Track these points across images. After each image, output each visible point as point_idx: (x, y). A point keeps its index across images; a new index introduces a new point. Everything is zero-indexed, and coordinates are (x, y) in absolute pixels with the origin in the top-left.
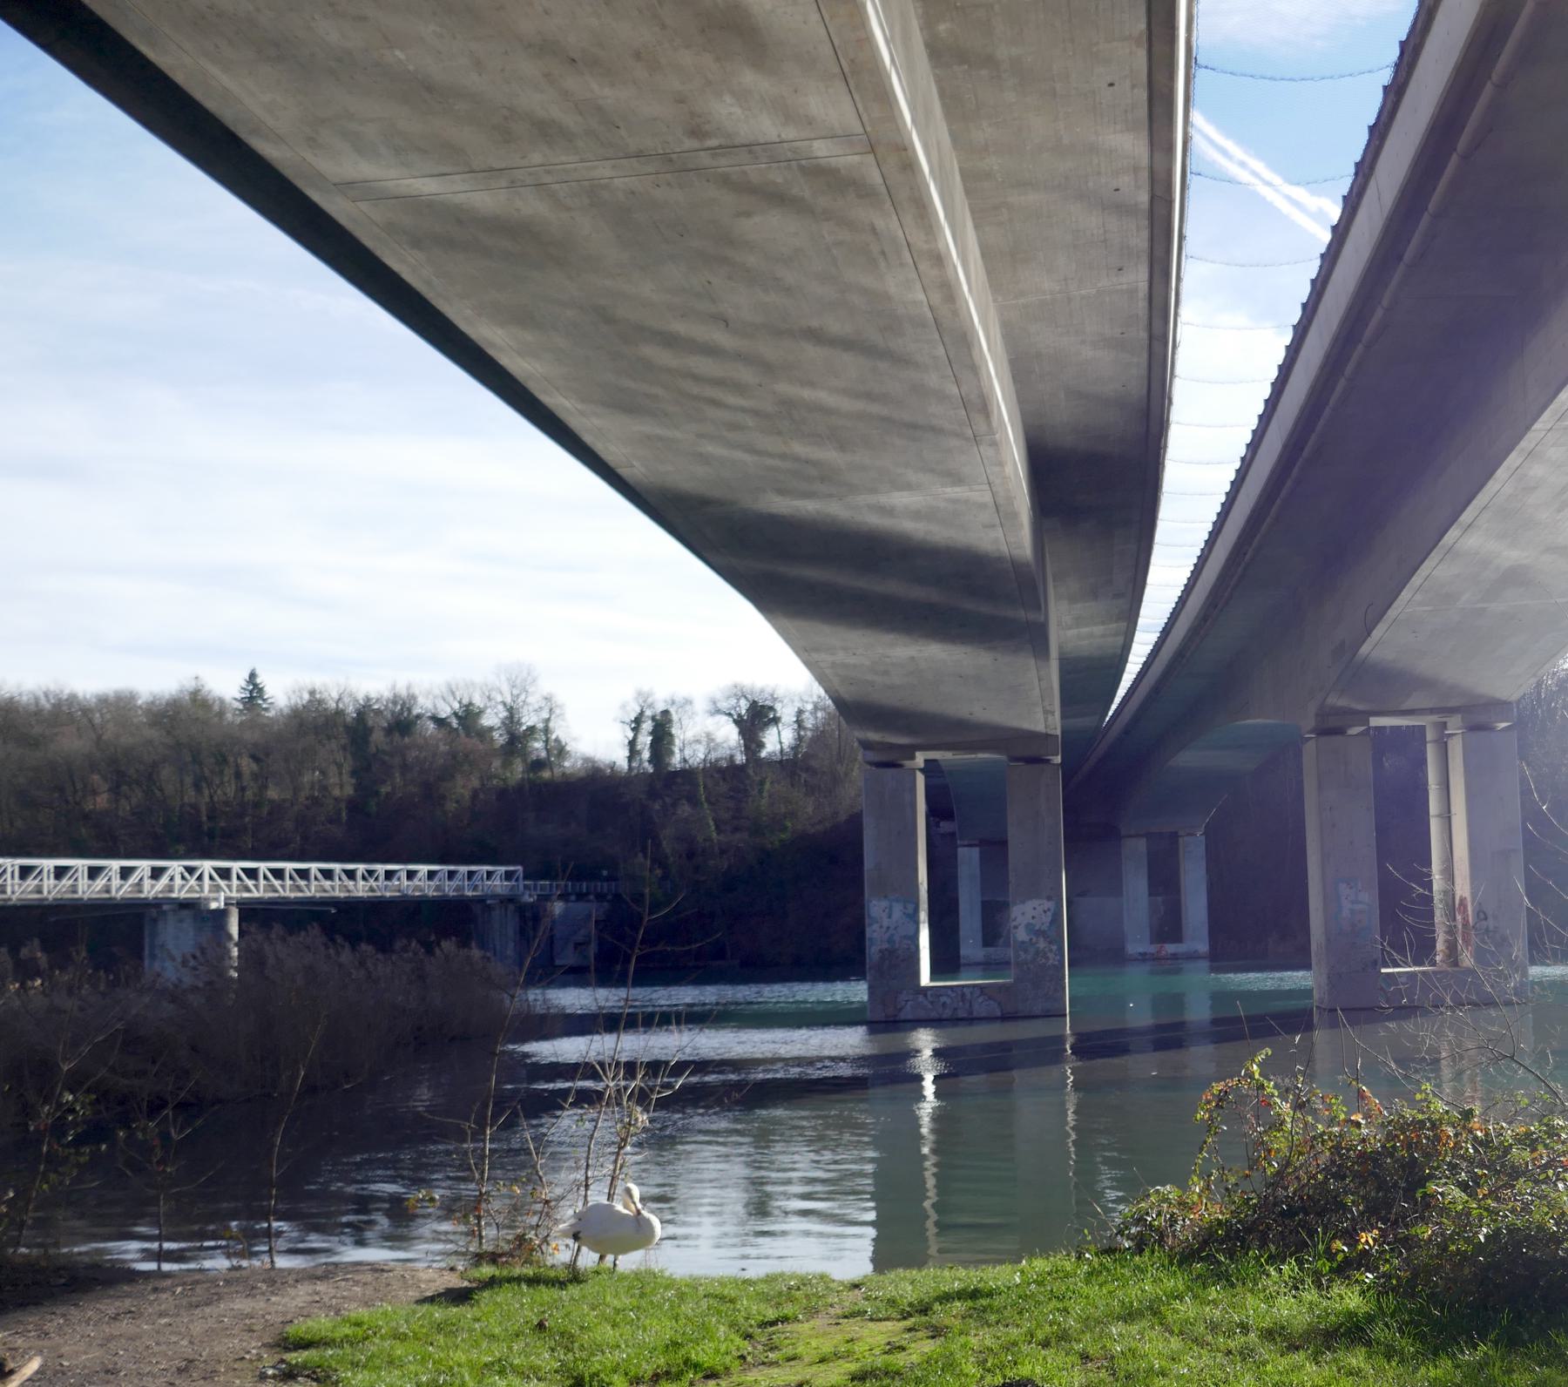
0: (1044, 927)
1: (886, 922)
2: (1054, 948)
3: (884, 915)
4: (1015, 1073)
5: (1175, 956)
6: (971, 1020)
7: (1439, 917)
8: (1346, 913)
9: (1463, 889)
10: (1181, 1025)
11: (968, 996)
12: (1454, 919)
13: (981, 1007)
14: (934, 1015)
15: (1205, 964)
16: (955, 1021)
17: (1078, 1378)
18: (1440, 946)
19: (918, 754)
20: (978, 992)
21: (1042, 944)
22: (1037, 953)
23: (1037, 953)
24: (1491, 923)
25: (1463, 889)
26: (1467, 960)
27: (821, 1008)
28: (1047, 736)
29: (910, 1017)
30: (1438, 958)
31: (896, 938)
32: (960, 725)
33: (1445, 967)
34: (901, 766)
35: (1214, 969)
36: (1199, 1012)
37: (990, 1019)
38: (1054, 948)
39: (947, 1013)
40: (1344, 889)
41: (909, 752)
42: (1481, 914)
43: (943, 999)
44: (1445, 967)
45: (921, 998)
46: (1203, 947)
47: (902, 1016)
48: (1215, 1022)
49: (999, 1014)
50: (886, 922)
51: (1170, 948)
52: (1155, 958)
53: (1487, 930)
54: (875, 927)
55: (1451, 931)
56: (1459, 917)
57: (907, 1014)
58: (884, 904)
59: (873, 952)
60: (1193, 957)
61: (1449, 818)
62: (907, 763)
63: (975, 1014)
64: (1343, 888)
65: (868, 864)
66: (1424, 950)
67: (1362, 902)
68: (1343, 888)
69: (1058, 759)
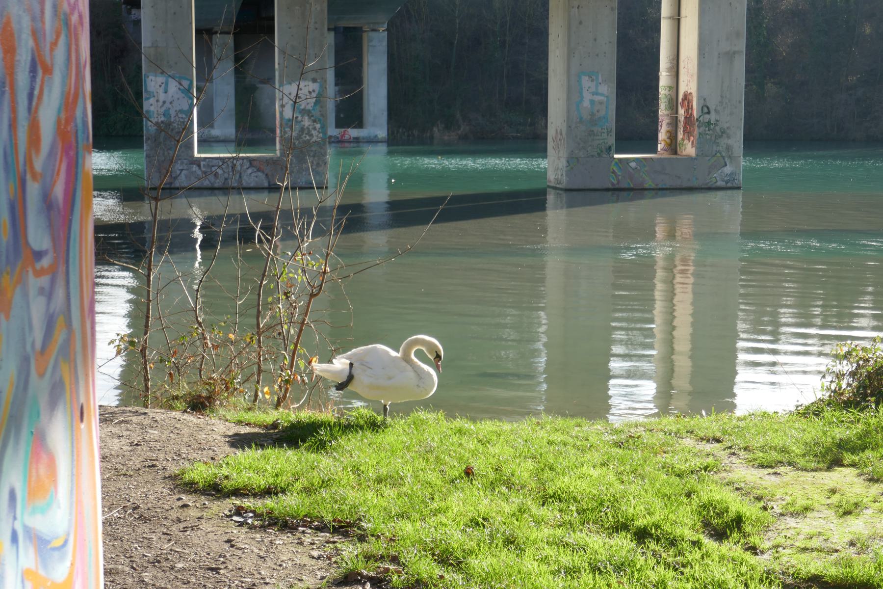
0: (309, 107)
1: (162, 97)
2: (318, 126)
3: (161, 90)
5: (357, 140)
7: (663, 110)
8: (586, 103)
9: (688, 84)
11: (238, 168)
12: (677, 112)
15: (383, 148)
17: (689, 586)
18: (662, 135)
20: (247, 164)
21: (307, 122)
22: (302, 130)
23: (302, 130)
24: (713, 117)
25: (688, 84)
26: (689, 149)
27: (110, 174)
29: (185, 184)
30: (660, 147)
33: (666, 155)
35: (390, 153)
36: (377, 193)
37: (257, 189)
39: (218, 183)
40: (585, 81)
42: (705, 109)
44: (666, 155)
45: (195, 168)
47: (177, 184)
49: (266, 185)
50: (162, 97)
51: (353, 133)
53: (709, 123)
54: (152, 101)
55: (674, 122)
56: (681, 111)
58: (161, 79)
59: (149, 128)
60: (373, 141)
61: (679, 20)
63: (245, 184)
64: (585, 80)
65: (146, 41)
66: (648, 141)
67: (601, 94)
68: (585, 80)
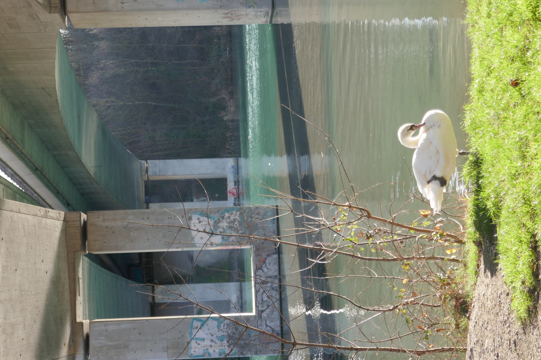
0: (212, 222)
1: (208, 343)
2: (227, 215)
3: (202, 344)
4: (285, 157)
5: (237, 183)
6: (280, 276)
10: (292, 178)
13: (271, 269)
14: (277, 305)
15: (242, 161)
16: (281, 289)
19: (78, 320)
20: (260, 272)
21: (224, 224)
22: (230, 227)
23: (230, 227)
28: (65, 220)
29: (278, 323)
31: (220, 334)
32: (56, 282)
34: (88, 336)
36: (279, 165)
38: (227, 215)
39: (275, 295)
41: (77, 327)
43: (265, 298)
45: (264, 315)
46: (230, 162)
47: (278, 329)
48: (289, 152)
49: (276, 256)
50: (208, 343)
51: (231, 186)
52: (238, 197)
54: (211, 351)
57: (276, 325)
58: (193, 344)
60: (237, 169)
62: (86, 330)
63: (277, 273)
69: (84, 216)
